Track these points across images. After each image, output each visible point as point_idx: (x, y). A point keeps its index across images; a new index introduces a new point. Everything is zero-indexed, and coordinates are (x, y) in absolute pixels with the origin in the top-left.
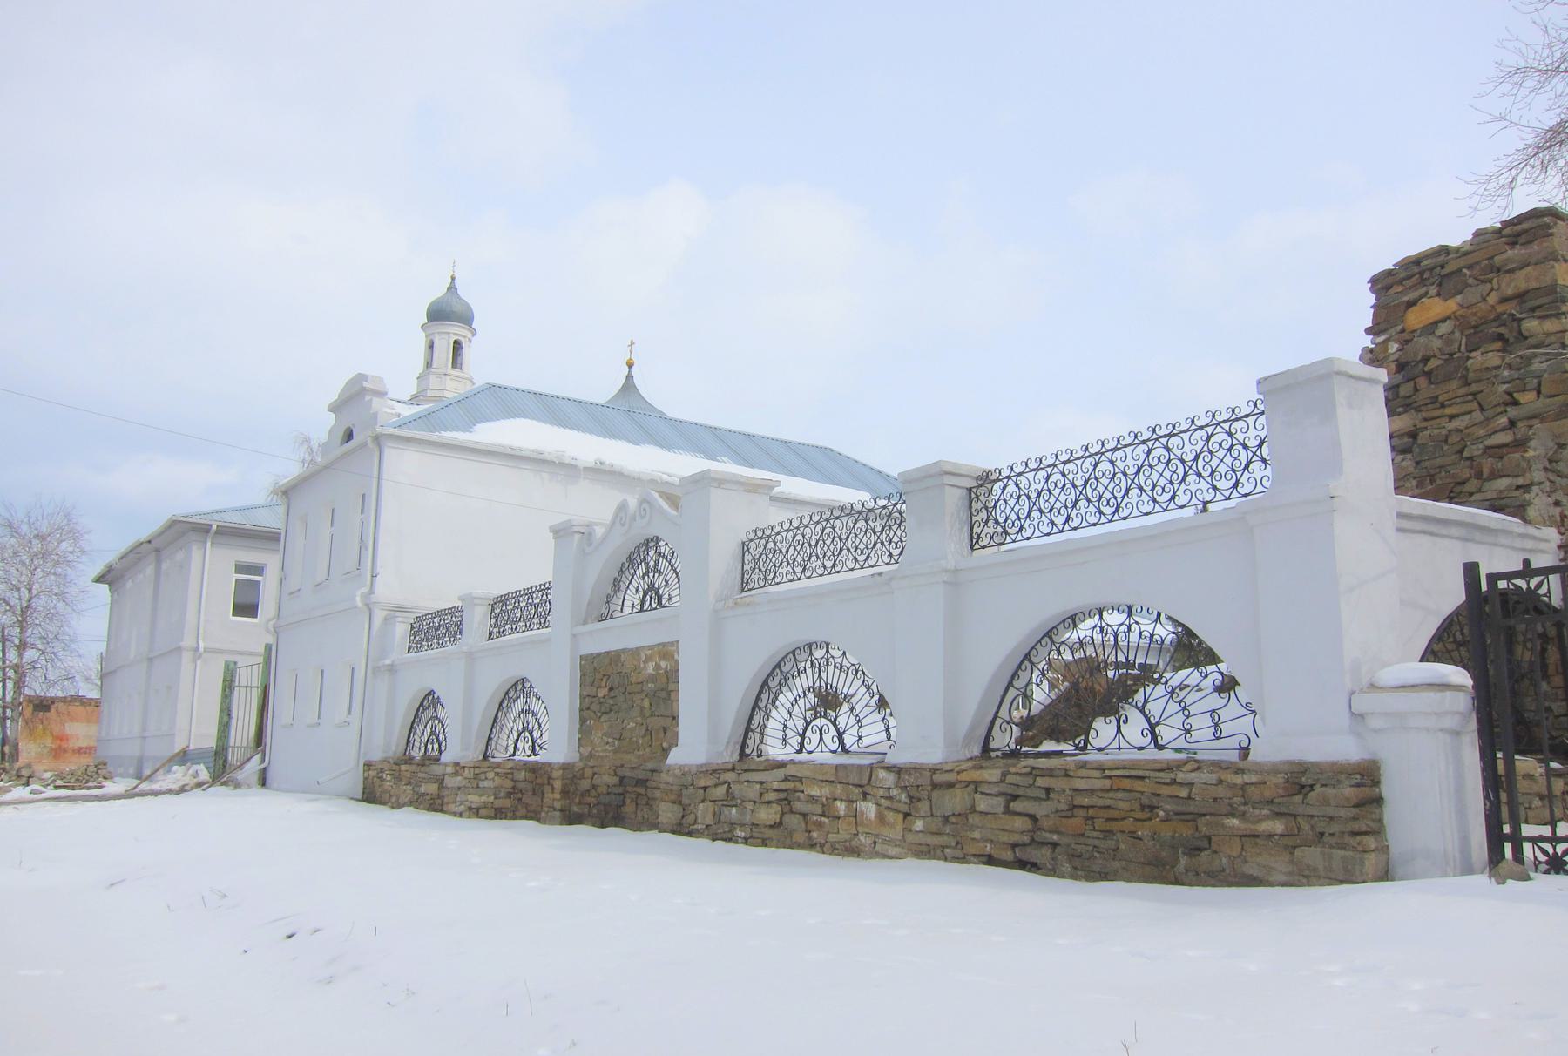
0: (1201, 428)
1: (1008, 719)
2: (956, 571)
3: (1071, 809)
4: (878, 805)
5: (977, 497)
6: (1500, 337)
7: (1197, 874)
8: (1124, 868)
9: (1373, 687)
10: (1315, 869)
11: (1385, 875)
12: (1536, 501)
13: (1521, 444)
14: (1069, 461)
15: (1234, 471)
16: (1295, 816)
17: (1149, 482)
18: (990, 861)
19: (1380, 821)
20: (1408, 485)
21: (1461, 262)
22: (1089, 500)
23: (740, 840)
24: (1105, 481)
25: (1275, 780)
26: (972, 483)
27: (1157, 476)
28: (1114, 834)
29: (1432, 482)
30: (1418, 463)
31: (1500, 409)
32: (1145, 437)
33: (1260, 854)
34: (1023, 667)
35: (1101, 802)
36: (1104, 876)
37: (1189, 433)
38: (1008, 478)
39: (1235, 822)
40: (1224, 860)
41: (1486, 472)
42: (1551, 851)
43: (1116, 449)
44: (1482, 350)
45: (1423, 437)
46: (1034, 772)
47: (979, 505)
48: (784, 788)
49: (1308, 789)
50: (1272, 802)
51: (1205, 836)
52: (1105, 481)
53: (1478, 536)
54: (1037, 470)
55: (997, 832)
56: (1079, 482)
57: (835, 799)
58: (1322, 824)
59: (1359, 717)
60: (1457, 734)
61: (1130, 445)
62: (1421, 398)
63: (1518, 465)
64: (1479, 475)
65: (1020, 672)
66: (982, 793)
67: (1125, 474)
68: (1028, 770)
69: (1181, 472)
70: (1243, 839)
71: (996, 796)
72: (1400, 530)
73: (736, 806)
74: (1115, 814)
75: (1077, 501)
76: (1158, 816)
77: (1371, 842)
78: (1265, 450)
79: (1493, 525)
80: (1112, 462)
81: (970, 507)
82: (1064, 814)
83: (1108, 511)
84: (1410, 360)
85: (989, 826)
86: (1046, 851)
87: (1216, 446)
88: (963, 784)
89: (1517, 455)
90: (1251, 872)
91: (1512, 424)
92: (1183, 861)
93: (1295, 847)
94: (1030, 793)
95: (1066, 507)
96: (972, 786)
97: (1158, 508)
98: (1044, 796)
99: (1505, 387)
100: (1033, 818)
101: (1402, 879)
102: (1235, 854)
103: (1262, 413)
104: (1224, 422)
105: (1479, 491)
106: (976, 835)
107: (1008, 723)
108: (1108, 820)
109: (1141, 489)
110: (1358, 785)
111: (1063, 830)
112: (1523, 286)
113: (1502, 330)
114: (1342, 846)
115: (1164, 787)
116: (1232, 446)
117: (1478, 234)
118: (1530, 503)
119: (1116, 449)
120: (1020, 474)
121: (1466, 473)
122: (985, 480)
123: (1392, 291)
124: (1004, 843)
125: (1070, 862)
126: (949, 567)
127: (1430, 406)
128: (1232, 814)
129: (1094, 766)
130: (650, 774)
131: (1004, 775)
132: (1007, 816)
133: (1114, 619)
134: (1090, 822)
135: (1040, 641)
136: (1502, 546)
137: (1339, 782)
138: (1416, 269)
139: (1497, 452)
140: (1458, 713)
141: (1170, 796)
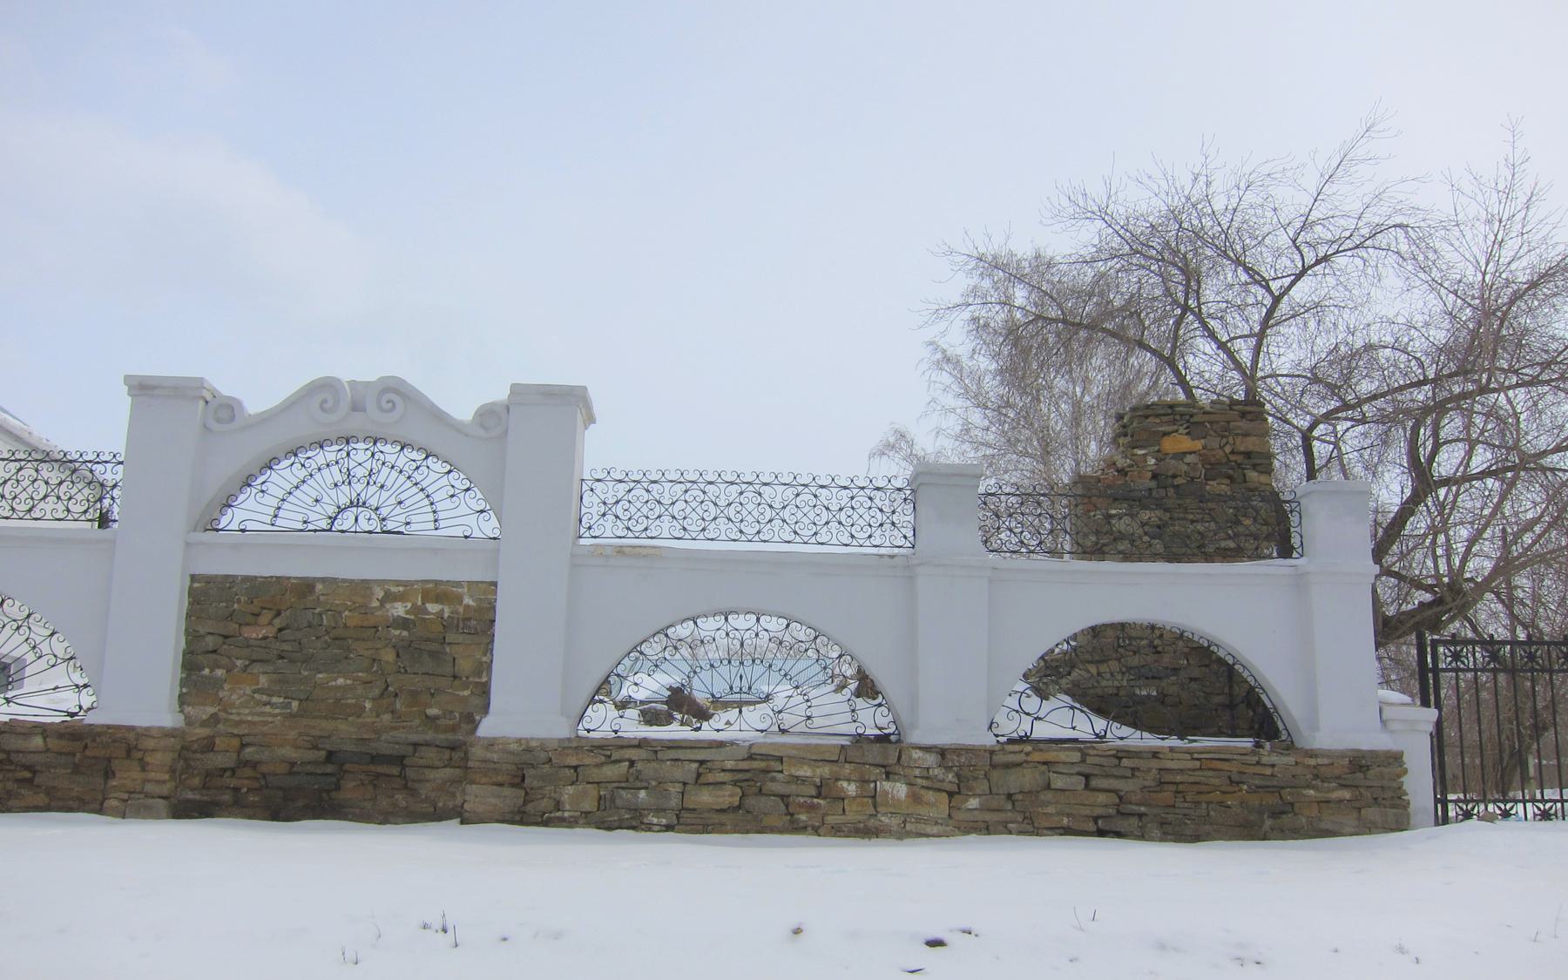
1: (1018, 708)
3: (1159, 786)
4: (910, 784)
6: (1230, 477)
7: (1282, 831)
8: (1215, 831)
16: (1357, 787)
18: (1067, 831)
21: (1206, 418)
23: (657, 828)
25: (1342, 763)
33: (1333, 814)
35: (1192, 779)
37: (6, 462)
42: (1542, 808)
44: (1218, 481)
48: (747, 768)
57: (837, 780)
70: (1321, 804)
73: (646, 788)
74: (1204, 788)
82: (1152, 790)
84: (1162, 473)
86: (1134, 821)
90: (1326, 827)
94: (1115, 771)
103: (121, 463)
108: (1199, 793)
112: (1251, 448)
113: (1231, 472)
115: (1251, 767)
128: (1308, 787)
130: (410, 749)
132: (1088, 793)
138: (1169, 411)
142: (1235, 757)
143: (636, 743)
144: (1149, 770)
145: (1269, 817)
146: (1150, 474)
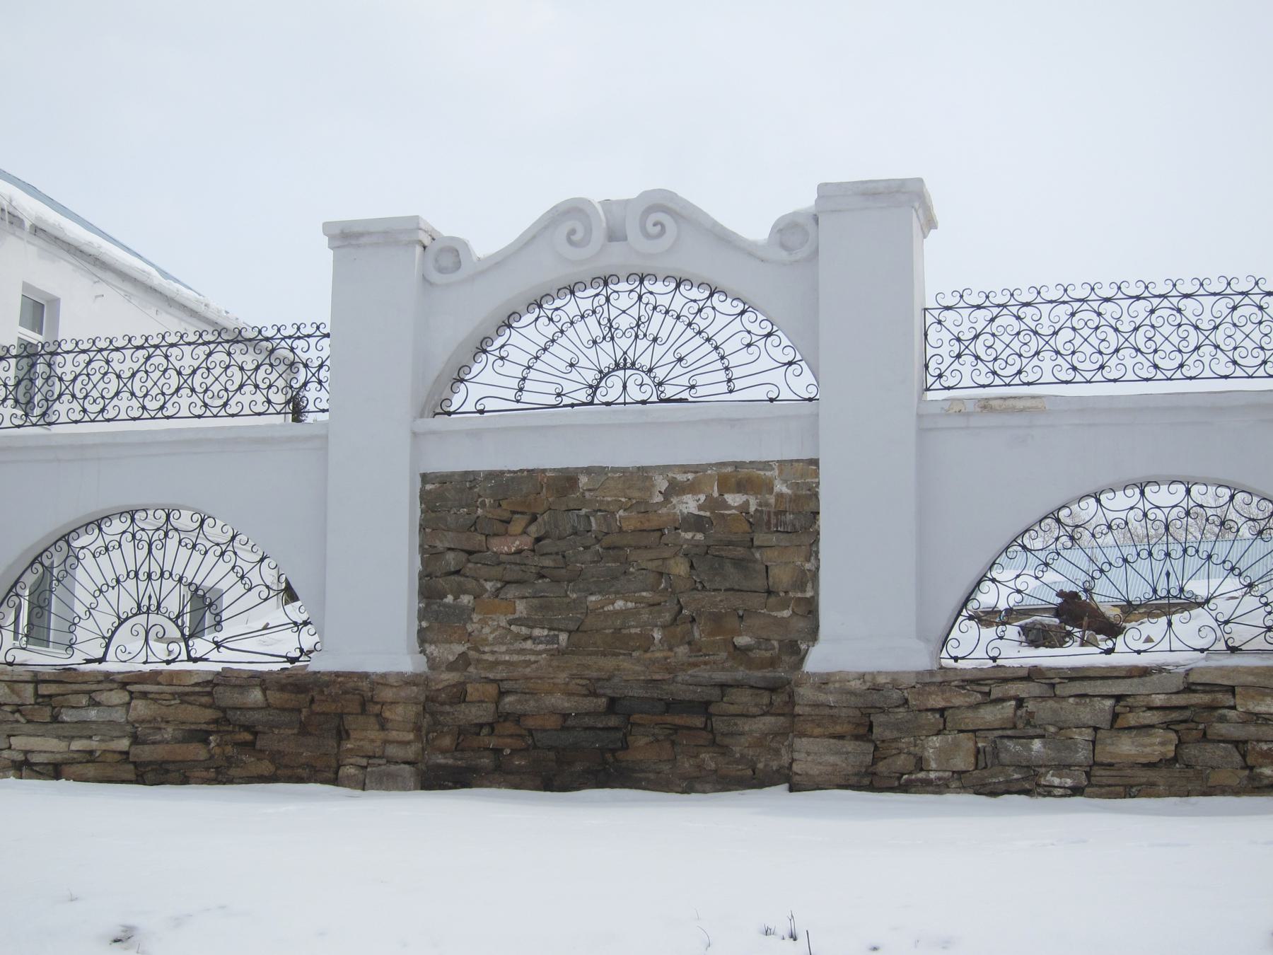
37: (193, 347)
38: (157, 347)
69: (78, 384)
73: (1041, 736)
78: (323, 374)
103: (328, 335)
120: (172, 345)
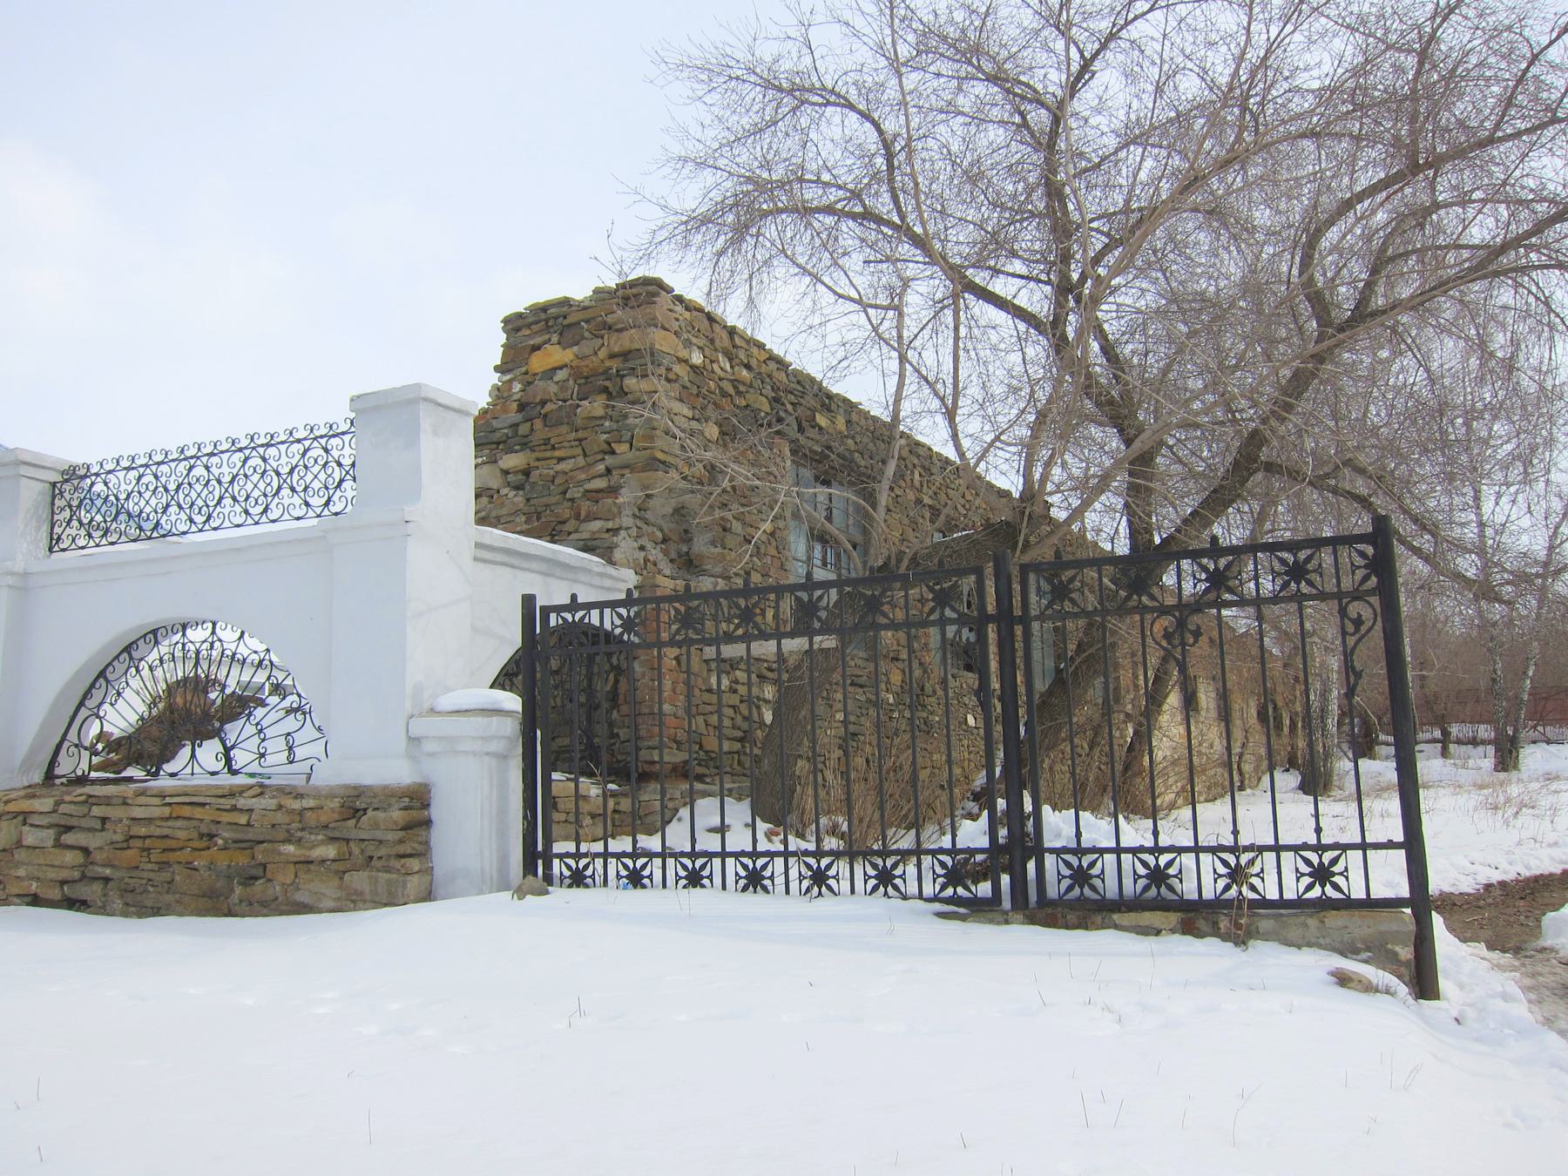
0: (299, 441)
2: (25, 575)
5: (61, 493)
6: (606, 390)
7: (251, 904)
9: (433, 711)
10: (362, 893)
11: (428, 896)
12: (623, 544)
13: (613, 491)
14: (163, 463)
15: (327, 488)
16: (348, 841)
17: (243, 492)
18: (36, 901)
19: (427, 843)
20: (518, 520)
21: (581, 316)
22: (180, 507)
24: (198, 487)
26: (57, 478)
27: (253, 486)
28: (170, 866)
29: (538, 519)
30: (528, 500)
31: (600, 457)
32: (243, 445)
34: (97, 685)
35: (158, 832)
36: (157, 911)
38: (97, 475)
39: (291, 848)
40: (277, 888)
41: (583, 514)
43: (212, 454)
45: (535, 475)
46: (90, 801)
47: (62, 503)
49: (361, 813)
50: (327, 827)
51: (259, 864)
52: (198, 487)
53: (558, 572)
54: (128, 469)
55: (45, 868)
56: (172, 487)
58: (372, 848)
59: (414, 741)
60: (503, 757)
61: (227, 451)
62: (536, 438)
63: (610, 510)
64: (577, 517)
65: (94, 691)
66: (32, 825)
67: (219, 482)
68: (83, 798)
69: (275, 485)
71: (48, 828)
72: (476, 559)
75: (168, 505)
76: (216, 845)
77: (415, 864)
79: (573, 562)
80: (207, 468)
81: (53, 504)
82: (118, 846)
83: (199, 519)
85: (36, 861)
86: (97, 887)
87: (312, 461)
88: (10, 816)
89: (610, 501)
91: (609, 471)
92: (238, 890)
93: (344, 872)
94: (85, 823)
95: (156, 512)
96: (20, 818)
97: (250, 521)
98: (99, 826)
99: (605, 436)
100: (86, 851)
101: (454, 896)
102: (289, 882)
104: (322, 437)
105: (576, 531)
106: (21, 872)
107: (76, 746)
108: (164, 850)
109: (234, 499)
110: (406, 808)
111: (116, 863)
112: (627, 345)
113: (607, 383)
114: (388, 870)
116: (327, 463)
117: (597, 291)
118: (617, 546)
119: (212, 454)
120: (110, 472)
121: (567, 514)
122: (73, 474)
123: (519, 334)
124: (51, 881)
125: (122, 897)
126: (16, 570)
127: (543, 447)
128: (288, 841)
129: (155, 792)
131: (57, 803)
133: (197, 635)
134: (145, 854)
135: (117, 657)
136: (581, 582)
137: (390, 805)
138: (543, 316)
139: (594, 496)
140: (504, 737)
141: (230, 823)
142: (208, 800)
143: (226, 792)
144: (121, 820)
145: (238, 883)
146: (515, 406)
